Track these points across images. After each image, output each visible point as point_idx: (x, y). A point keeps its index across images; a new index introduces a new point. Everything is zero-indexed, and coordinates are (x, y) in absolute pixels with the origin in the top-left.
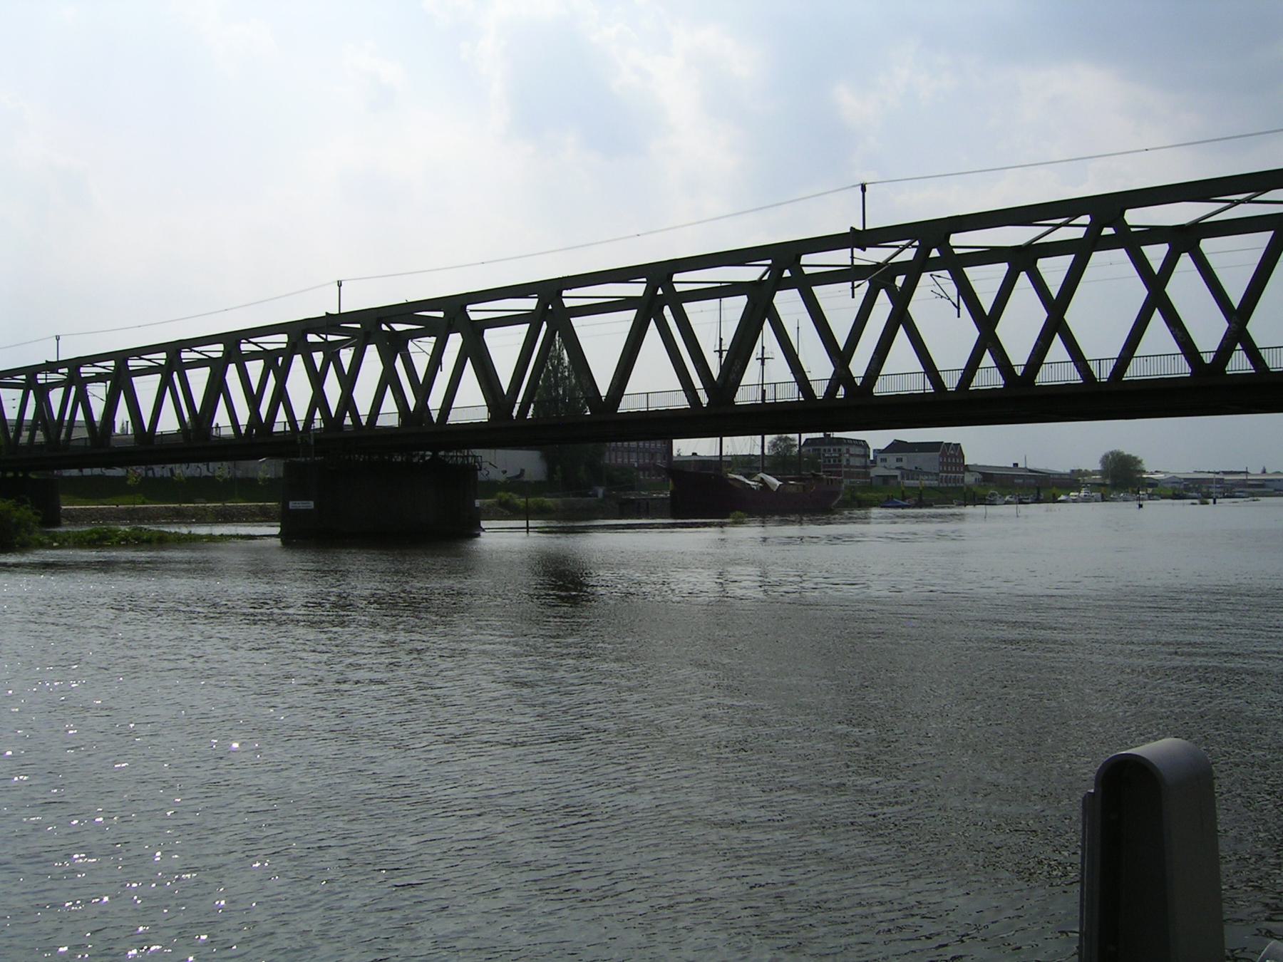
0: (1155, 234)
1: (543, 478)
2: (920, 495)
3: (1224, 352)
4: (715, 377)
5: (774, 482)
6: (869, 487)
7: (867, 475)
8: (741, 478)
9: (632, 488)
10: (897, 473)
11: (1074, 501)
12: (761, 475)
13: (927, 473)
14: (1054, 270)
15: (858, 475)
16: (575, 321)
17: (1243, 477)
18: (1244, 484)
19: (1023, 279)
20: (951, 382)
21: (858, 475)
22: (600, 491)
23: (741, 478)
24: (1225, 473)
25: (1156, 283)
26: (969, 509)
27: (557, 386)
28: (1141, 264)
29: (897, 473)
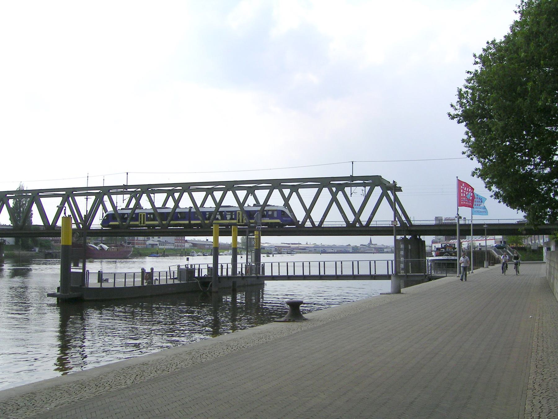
0: (334, 185)
1: (13, 244)
2: (164, 252)
3: (304, 222)
4: (422, 237)
5: (106, 247)
6: (146, 248)
7: (145, 244)
8: (93, 245)
9: (50, 249)
10: (158, 243)
11: (226, 255)
12: (101, 244)
13: (170, 243)
14: (177, 195)
15: (141, 244)
16: (42, 199)
17: (297, 246)
18: (298, 248)
19: (294, 194)
20: (317, 224)
21: (141, 244)
22: (37, 249)
23: (93, 245)
24: (292, 244)
25: (334, 195)
26: (95, 260)
27: (20, 207)
28: (331, 191)
29: (158, 243)
